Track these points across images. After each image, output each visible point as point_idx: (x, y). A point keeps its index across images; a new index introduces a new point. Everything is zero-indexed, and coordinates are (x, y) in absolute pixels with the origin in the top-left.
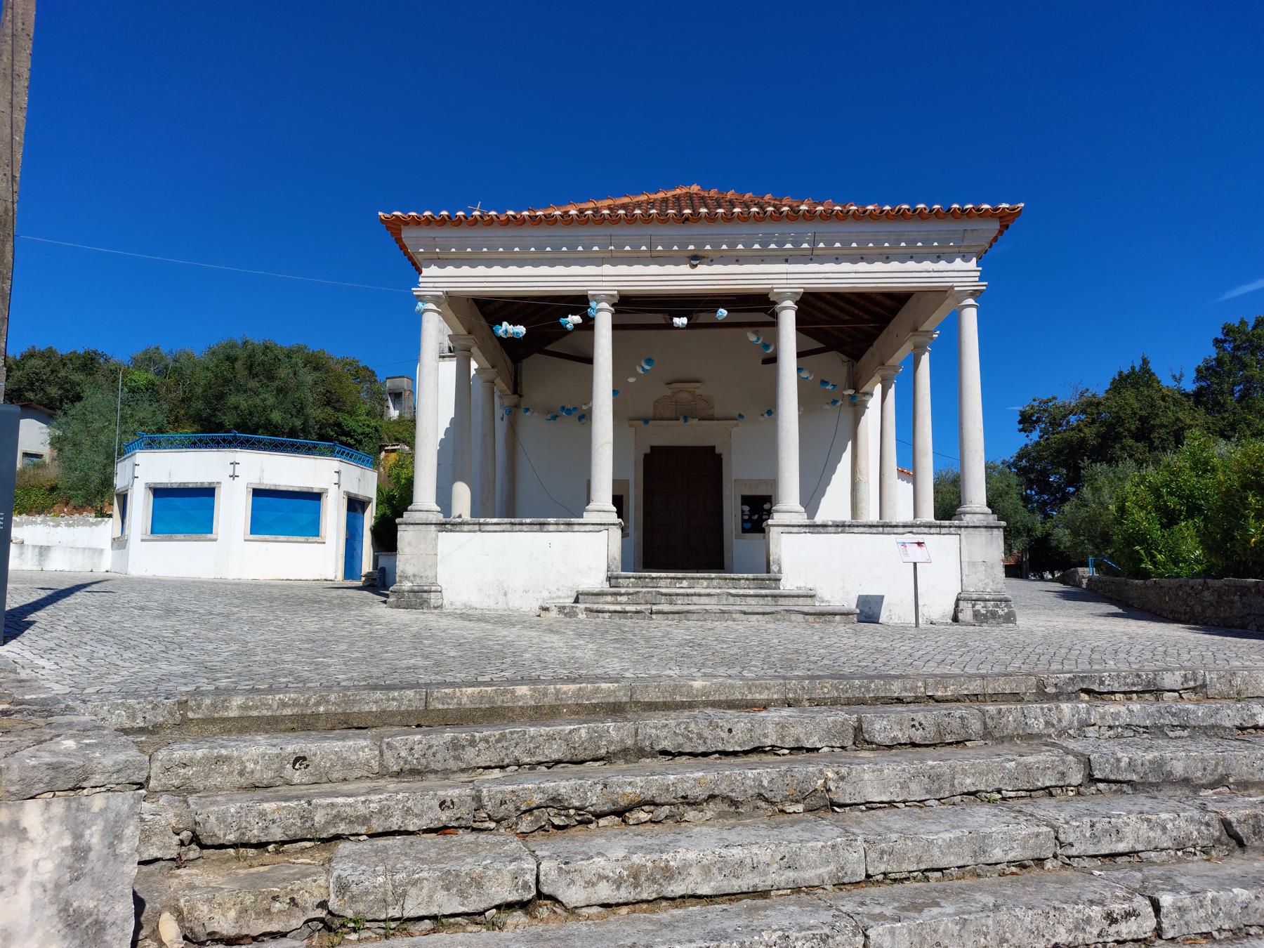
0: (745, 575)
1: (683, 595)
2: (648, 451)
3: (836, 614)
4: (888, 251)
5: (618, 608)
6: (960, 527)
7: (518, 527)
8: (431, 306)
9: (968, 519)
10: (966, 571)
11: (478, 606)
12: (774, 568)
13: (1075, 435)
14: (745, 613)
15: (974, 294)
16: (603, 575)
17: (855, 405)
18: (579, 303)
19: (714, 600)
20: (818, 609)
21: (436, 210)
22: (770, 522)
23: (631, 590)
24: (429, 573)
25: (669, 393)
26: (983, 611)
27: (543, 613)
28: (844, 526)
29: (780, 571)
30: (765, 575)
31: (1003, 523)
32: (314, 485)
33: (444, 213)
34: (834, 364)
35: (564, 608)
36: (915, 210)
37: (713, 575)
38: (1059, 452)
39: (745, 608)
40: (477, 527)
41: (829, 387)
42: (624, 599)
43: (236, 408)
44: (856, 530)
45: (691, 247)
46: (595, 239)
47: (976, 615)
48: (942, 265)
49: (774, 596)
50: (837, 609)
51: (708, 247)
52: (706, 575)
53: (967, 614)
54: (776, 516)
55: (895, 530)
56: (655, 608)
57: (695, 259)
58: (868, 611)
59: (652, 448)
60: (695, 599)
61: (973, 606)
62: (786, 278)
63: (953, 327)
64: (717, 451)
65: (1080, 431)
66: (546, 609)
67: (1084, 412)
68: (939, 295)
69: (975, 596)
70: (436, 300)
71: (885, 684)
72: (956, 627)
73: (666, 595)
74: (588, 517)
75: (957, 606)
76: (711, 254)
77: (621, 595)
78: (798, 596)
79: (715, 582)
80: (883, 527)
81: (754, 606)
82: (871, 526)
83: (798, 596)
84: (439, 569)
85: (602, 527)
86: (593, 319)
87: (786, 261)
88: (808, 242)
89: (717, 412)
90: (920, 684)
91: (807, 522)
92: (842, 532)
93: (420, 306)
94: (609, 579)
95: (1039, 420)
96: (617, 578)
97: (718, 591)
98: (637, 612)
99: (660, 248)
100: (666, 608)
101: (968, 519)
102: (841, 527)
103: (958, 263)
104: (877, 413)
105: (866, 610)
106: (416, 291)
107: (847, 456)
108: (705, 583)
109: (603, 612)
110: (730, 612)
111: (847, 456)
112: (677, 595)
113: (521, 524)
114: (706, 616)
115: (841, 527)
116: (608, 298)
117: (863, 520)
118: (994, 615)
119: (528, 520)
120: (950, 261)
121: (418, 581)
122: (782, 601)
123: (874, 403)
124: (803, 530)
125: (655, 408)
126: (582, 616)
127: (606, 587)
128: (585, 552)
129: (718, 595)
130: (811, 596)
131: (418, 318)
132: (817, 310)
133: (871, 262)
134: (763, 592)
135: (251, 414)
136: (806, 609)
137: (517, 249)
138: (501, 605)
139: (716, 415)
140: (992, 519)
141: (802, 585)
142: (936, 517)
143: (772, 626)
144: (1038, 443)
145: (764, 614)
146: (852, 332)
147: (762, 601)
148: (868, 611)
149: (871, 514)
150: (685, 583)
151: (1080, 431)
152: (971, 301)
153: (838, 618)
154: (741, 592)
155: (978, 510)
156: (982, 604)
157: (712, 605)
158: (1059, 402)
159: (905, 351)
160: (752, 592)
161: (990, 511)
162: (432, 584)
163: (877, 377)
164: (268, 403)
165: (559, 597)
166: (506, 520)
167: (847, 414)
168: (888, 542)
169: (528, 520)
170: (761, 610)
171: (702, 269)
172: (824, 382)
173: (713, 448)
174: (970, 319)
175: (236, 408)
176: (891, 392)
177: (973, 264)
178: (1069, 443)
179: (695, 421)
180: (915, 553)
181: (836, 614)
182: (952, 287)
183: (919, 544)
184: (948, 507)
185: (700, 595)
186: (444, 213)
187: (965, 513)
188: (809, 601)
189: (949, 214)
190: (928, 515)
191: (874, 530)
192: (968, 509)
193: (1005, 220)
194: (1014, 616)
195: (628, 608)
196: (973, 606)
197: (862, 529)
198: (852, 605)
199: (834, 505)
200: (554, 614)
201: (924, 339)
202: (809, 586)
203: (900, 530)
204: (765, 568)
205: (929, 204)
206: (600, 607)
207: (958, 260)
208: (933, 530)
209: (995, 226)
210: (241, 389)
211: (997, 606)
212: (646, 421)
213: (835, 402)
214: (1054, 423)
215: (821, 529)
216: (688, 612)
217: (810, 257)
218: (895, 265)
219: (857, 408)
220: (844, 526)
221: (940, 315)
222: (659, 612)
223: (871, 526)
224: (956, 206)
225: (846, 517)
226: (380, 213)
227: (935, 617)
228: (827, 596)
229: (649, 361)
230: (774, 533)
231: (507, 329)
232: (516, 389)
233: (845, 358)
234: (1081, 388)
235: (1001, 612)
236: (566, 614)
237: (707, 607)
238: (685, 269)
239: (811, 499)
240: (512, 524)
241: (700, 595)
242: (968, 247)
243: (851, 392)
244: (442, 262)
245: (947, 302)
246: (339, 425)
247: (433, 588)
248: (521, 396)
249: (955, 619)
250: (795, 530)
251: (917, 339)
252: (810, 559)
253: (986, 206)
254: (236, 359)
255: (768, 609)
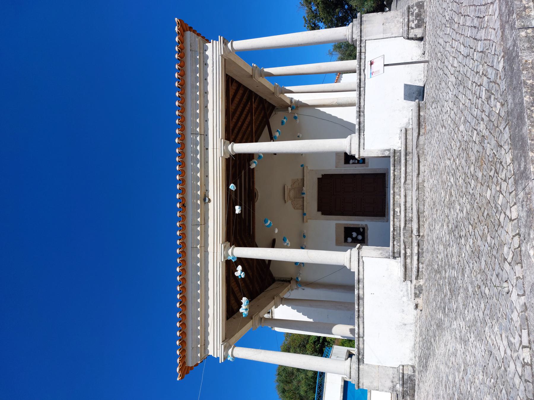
0: (392, 172)
1: (405, 213)
2: (320, 213)
3: (419, 115)
4: (202, 93)
5: (415, 258)
6: (361, 41)
7: (361, 313)
8: (230, 352)
9: (356, 37)
10: (389, 35)
11: (413, 343)
12: (387, 154)
13: (321, 5)
14: (419, 174)
15: (225, 43)
16: (392, 261)
17: (297, 107)
18: (230, 266)
19: (409, 193)
20: (415, 126)
21: (176, 347)
22: (357, 157)
23: (402, 246)
24: (391, 372)
25: (290, 202)
26: (416, 22)
27: (420, 308)
28: (360, 112)
29: (389, 150)
30: (392, 160)
31: (359, 15)
32: (339, 385)
33: (178, 343)
34: (275, 120)
35: (415, 294)
36: (179, 78)
37: (392, 192)
38: (328, 13)
39: (415, 174)
40: (361, 339)
41: (285, 120)
42: (408, 251)
43: (306, 392)
44: (362, 104)
45: (199, 202)
46: (194, 257)
47: (418, 26)
48: (209, 62)
49: (406, 155)
50: (415, 114)
51: (199, 193)
52: (391, 196)
53: (418, 32)
54: (353, 153)
55: (362, 79)
56: (415, 232)
57: (205, 199)
58: (416, 93)
59: (318, 210)
60: (408, 205)
61: (412, 28)
62: (215, 149)
63: (246, 54)
64: (320, 177)
65: (318, 4)
66: (417, 306)
67: (310, 3)
68: (226, 62)
69: (406, 28)
70: (226, 349)
71: (527, 69)
72: (427, 38)
73: (405, 224)
74: (354, 268)
75: (412, 39)
76: (203, 191)
77: (406, 253)
78: (406, 139)
79: (397, 190)
80: (360, 87)
81: (412, 167)
82: (360, 95)
83: (406, 139)
84: (388, 365)
85: (361, 260)
86: (238, 258)
87: (207, 149)
88: (196, 137)
89: (300, 177)
90: (523, 34)
91: (357, 134)
92: (364, 112)
93: (230, 358)
94: (394, 258)
95: (314, 24)
96: (394, 253)
97: (402, 190)
98: (419, 245)
99: (199, 220)
100: (415, 226)
101: (356, 37)
102: (360, 113)
103: (209, 53)
104: (300, 95)
105: (415, 95)
106: (221, 360)
107: (322, 109)
108: (397, 197)
109: (418, 268)
110: (418, 184)
111: (322, 109)
112: (405, 216)
113: (359, 311)
114: (421, 199)
115: (360, 113)
116: (226, 249)
117: (356, 100)
118: (418, 15)
119: (356, 307)
120: (207, 57)
121: (396, 380)
122: (409, 150)
123: (296, 97)
124: (362, 136)
125: (297, 209)
126: (422, 282)
127: (401, 260)
128: (377, 271)
129: (405, 190)
130: (406, 130)
131: (237, 361)
132: (233, 132)
133: (207, 101)
134: (403, 161)
135: (309, 385)
136: (415, 134)
137: (199, 309)
138: (413, 328)
139: (301, 177)
140: (356, 21)
141: (398, 136)
142: (355, 58)
143: (429, 158)
144: (324, 23)
145: (419, 162)
146: (252, 110)
147: (409, 162)
148: (416, 93)
149: (353, 96)
150: (397, 209)
151: (318, 4)
152: (229, 45)
153: (422, 114)
154: (403, 175)
155: (350, 31)
156: (411, 23)
157: (413, 195)
158: (306, 16)
159: (264, 81)
160: (403, 169)
161: (351, 24)
162: (398, 371)
163: (281, 96)
164: (304, 377)
165: (407, 290)
166: (356, 321)
167: (301, 111)
168: (370, 84)
169: (356, 307)
170: (416, 164)
171: (211, 196)
172: (282, 123)
173: (318, 179)
174: (239, 45)
175: (306, 392)
176: (288, 88)
177: (209, 45)
178: (324, 9)
179: (304, 189)
180: (378, 65)
181: (419, 115)
182: (222, 56)
183: (371, 63)
184: (348, 50)
185: (406, 202)
186: (178, 343)
187: (352, 38)
188: (409, 132)
189: (182, 60)
190: (352, 64)
191: (362, 93)
192: (350, 37)
193: (184, 28)
194: (419, 2)
195: (415, 251)
196: (412, 28)
197: (362, 100)
198: (413, 104)
199: (348, 115)
200: (420, 301)
201: (256, 72)
202: (399, 131)
203: (362, 77)
204: (388, 159)
205: (175, 71)
206: (415, 270)
207: (207, 53)
208: (363, 57)
209: (189, 34)
210: (297, 388)
211: (412, 14)
212: (304, 214)
213: (295, 118)
214: (315, 16)
215: (362, 125)
216: (418, 212)
217: (205, 135)
218: (210, 88)
219: (299, 106)
220: (360, 112)
221: (241, 63)
222: (419, 231)
223: (360, 95)
224: (176, 56)
225: (354, 109)
226: (178, 379)
227: (420, 52)
228: (406, 120)
229: (266, 221)
230: (364, 154)
231: (243, 310)
232: (288, 281)
233: (274, 113)
234: (300, 5)
235: (417, 11)
236: (420, 293)
237: (415, 198)
238: (211, 205)
239: (343, 129)
240: (359, 317)
241: (406, 202)
242: (200, 48)
243: (290, 109)
244: (205, 343)
245: (233, 59)
246: (315, 342)
247: (401, 371)
248: (292, 279)
249: (421, 39)
250: (362, 141)
251: (257, 76)
252: (381, 134)
253: (177, 39)
254: (284, 389)
255: (416, 159)
